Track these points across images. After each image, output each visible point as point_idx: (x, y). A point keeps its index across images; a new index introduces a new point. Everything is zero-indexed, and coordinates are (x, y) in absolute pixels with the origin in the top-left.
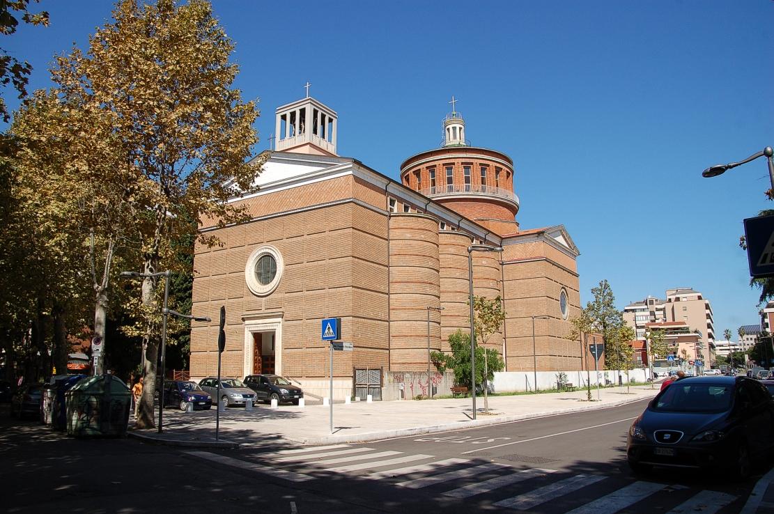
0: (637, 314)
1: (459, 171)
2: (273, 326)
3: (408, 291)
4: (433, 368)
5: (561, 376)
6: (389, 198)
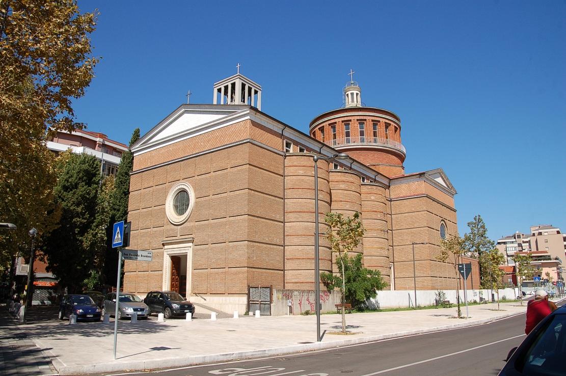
0: (508, 245)
1: (355, 127)
2: (185, 250)
3: (301, 219)
4: (322, 287)
5: (439, 294)
6: (285, 141)
